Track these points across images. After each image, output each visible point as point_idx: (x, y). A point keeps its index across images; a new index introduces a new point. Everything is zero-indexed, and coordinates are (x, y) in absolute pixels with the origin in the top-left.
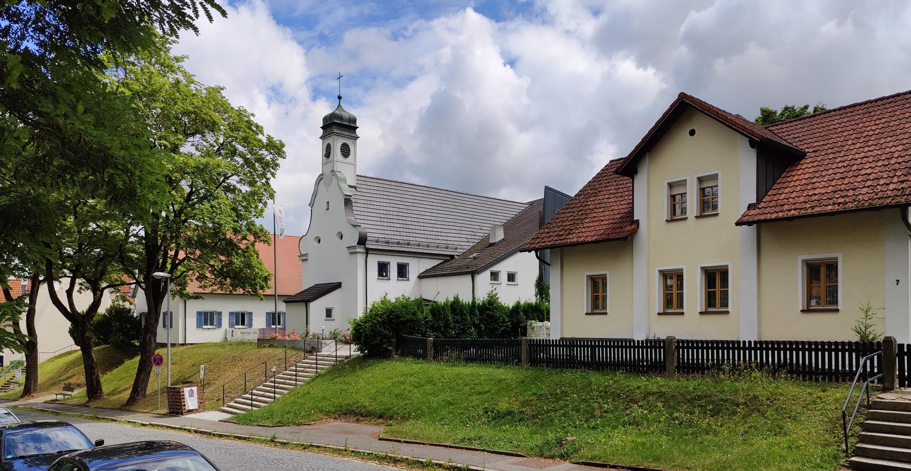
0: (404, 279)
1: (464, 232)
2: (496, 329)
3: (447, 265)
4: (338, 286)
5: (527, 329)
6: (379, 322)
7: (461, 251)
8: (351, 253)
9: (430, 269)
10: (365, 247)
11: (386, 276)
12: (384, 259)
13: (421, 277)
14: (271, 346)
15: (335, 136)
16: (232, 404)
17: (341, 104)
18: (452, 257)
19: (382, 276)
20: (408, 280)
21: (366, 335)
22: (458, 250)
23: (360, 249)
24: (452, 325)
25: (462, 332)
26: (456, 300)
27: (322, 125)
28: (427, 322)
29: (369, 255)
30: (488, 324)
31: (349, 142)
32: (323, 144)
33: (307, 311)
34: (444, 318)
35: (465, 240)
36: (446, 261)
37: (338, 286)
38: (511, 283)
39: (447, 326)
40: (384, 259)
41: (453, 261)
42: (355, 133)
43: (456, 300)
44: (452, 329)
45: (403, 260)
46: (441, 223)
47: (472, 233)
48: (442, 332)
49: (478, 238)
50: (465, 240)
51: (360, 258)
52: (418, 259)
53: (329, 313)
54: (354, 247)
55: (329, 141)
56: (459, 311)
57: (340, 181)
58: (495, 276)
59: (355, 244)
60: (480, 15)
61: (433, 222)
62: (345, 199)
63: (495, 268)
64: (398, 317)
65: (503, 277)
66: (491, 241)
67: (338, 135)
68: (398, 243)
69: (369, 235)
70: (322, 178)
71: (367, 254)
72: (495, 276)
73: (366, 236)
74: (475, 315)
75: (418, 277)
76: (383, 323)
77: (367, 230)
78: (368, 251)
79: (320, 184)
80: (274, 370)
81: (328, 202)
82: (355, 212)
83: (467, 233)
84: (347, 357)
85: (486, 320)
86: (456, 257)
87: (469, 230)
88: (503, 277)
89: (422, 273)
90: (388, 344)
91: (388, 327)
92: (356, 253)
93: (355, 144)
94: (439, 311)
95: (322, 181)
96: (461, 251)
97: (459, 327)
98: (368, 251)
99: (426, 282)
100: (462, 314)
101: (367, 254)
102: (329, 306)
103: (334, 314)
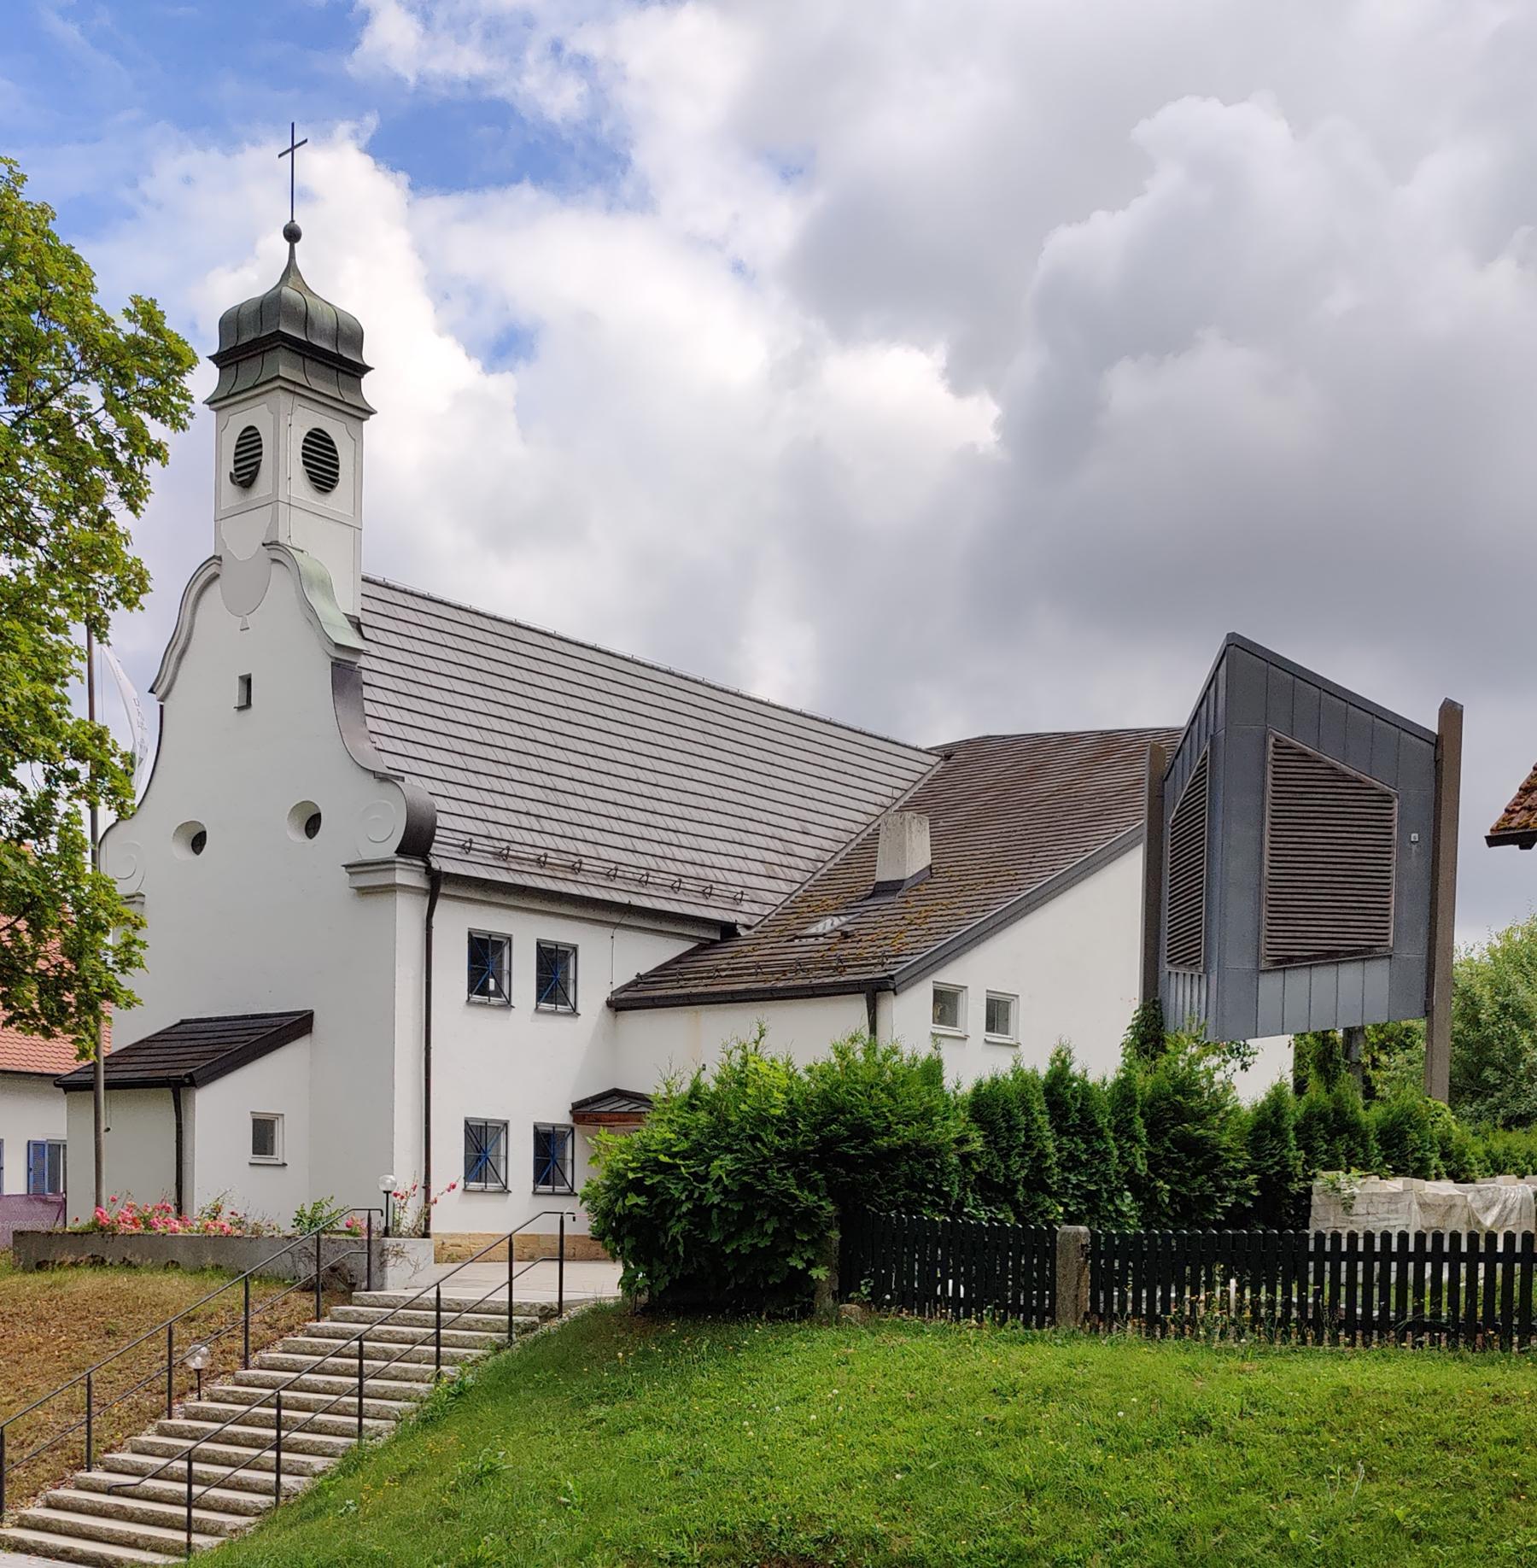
0: (561, 1008)
1: (754, 839)
2: (1207, 1202)
3: (719, 958)
4: (298, 1026)
5: (1309, 1207)
6: (778, 1152)
7: (756, 908)
8: (364, 891)
9: (647, 976)
10: (429, 870)
11: (499, 992)
12: (492, 921)
13: (619, 1004)
14: (98, 1262)
15: (282, 397)
16: (37, 1512)
17: (300, 262)
18: (728, 931)
19: (483, 991)
20: (574, 1012)
21: (701, 1212)
22: (746, 907)
23: (408, 875)
24: (1054, 1179)
25: (1089, 1211)
26: (1059, 1077)
27: (214, 350)
28: (965, 1159)
29: (441, 905)
30: (1182, 1181)
31: (335, 428)
32: (220, 430)
33: (179, 1126)
34: (1028, 1146)
35: (761, 868)
36: (705, 946)
37: (298, 1026)
38: (995, 1037)
39: (1037, 1183)
40: (492, 921)
41: (732, 947)
42: (357, 390)
43: (1059, 1077)
44: (1052, 1194)
45: (560, 932)
46: (674, 796)
47: (778, 845)
48: (1015, 1206)
49: (801, 864)
50: (761, 868)
51: (407, 912)
52: (609, 931)
53: (263, 1135)
54: (384, 865)
55: (256, 414)
56: (1075, 1118)
57: (311, 585)
58: (946, 1004)
59: (388, 850)
60: (466, 193)
61: (645, 790)
62: (337, 665)
63: (949, 976)
64: (862, 1132)
65: (973, 1012)
66: (884, 874)
67: (294, 389)
68: (541, 863)
69: (442, 820)
70: (215, 577)
71: (433, 896)
72: (946, 1004)
73: (434, 827)
74: (1134, 1139)
75: (609, 1004)
76: (792, 1158)
77: (441, 804)
78: (437, 885)
79: (207, 595)
80: (196, 1363)
81: (247, 681)
82: (372, 724)
83: (763, 842)
84: (547, 1313)
85: (1174, 1163)
86: (743, 932)
87: (769, 830)
88: (973, 1012)
89: (625, 988)
90: (809, 1255)
91: (817, 1175)
92: (391, 889)
93: (357, 440)
94: (1008, 1115)
95: (215, 589)
96: (756, 908)
97: (1077, 1186)
98: (437, 885)
99: (639, 1023)
100: (1088, 1128)
101: (433, 896)
102: (266, 1108)
103: (286, 1140)
